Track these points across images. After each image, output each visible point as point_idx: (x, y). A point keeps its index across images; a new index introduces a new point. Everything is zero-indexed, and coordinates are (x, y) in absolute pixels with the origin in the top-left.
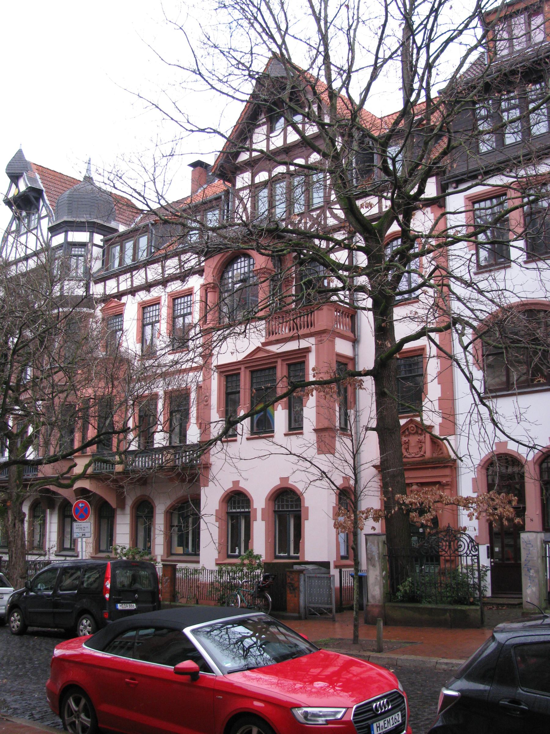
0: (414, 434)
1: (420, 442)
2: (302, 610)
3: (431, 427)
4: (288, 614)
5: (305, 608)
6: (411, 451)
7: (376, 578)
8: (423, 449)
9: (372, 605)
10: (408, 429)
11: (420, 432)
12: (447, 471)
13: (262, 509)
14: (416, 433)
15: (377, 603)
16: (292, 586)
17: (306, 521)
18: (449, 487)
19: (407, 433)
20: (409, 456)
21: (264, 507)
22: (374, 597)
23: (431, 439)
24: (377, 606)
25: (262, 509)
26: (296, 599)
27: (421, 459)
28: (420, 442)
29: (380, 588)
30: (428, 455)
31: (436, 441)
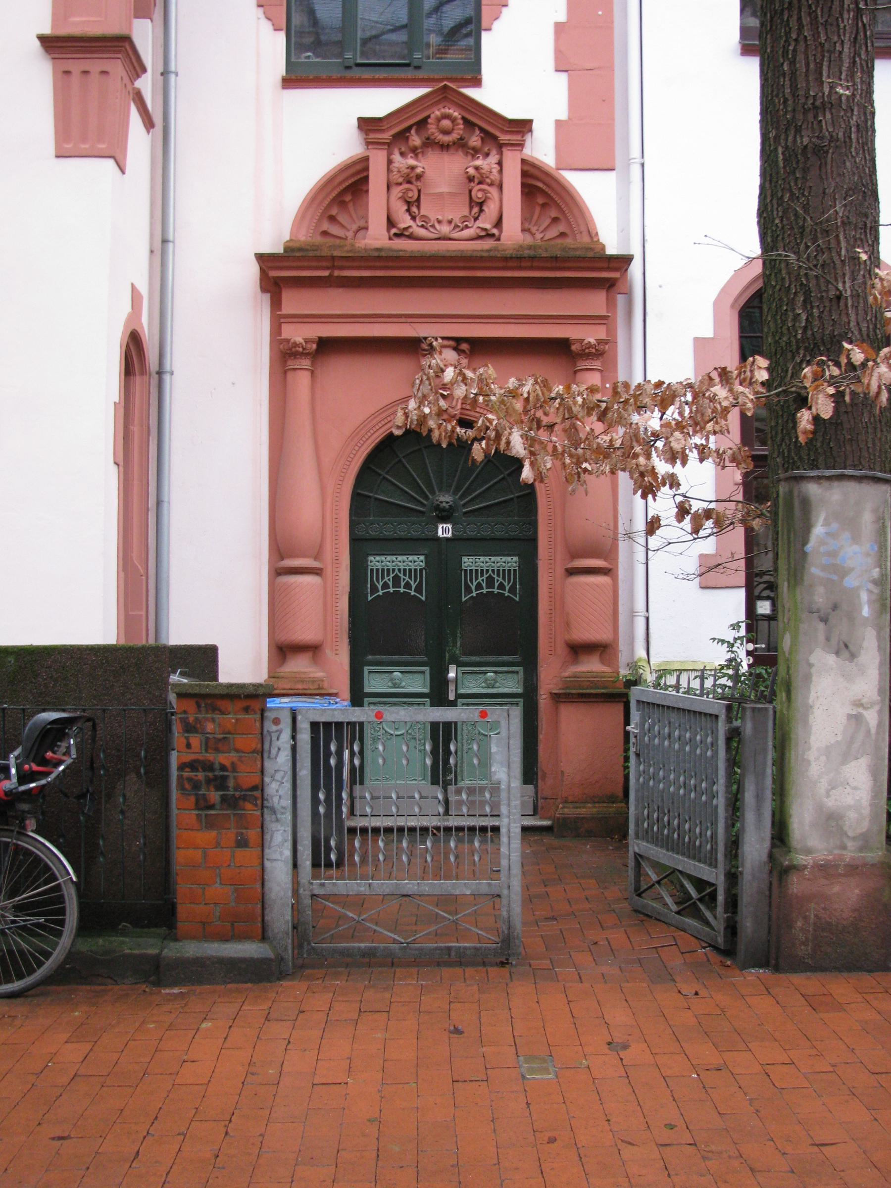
0: (444, 147)
1: (476, 179)
2: (280, 917)
3: (523, 126)
4: (191, 949)
5: (296, 909)
6: (427, 209)
7: (856, 719)
8: (491, 209)
9: (825, 869)
10: (422, 124)
11: (475, 140)
12: (593, 302)
13: (559, 123)
14: (461, 145)
15: (851, 852)
16: (220, 783)
17: (707, 331)
18: (597, 364)
19: (416, 140)
20: (422, 232)
21: (563, 115)
22: (831, 821)
23: (524, 174)
24: (853, 869)
25: (559, 123)
26: (247, 855)
27: (488, 244)
28: (476, 179)
29: (874, 773)
30: (513, 233)
31: (542, 190)
